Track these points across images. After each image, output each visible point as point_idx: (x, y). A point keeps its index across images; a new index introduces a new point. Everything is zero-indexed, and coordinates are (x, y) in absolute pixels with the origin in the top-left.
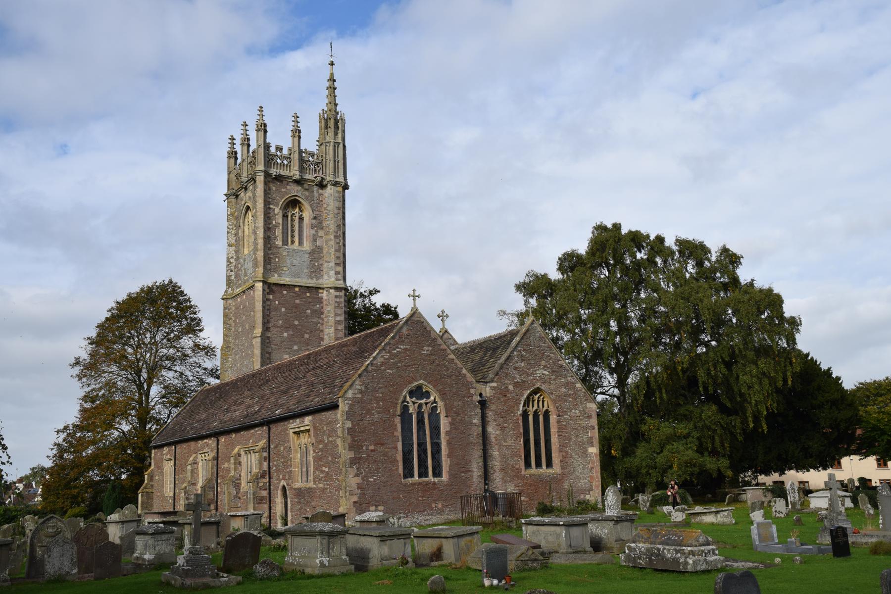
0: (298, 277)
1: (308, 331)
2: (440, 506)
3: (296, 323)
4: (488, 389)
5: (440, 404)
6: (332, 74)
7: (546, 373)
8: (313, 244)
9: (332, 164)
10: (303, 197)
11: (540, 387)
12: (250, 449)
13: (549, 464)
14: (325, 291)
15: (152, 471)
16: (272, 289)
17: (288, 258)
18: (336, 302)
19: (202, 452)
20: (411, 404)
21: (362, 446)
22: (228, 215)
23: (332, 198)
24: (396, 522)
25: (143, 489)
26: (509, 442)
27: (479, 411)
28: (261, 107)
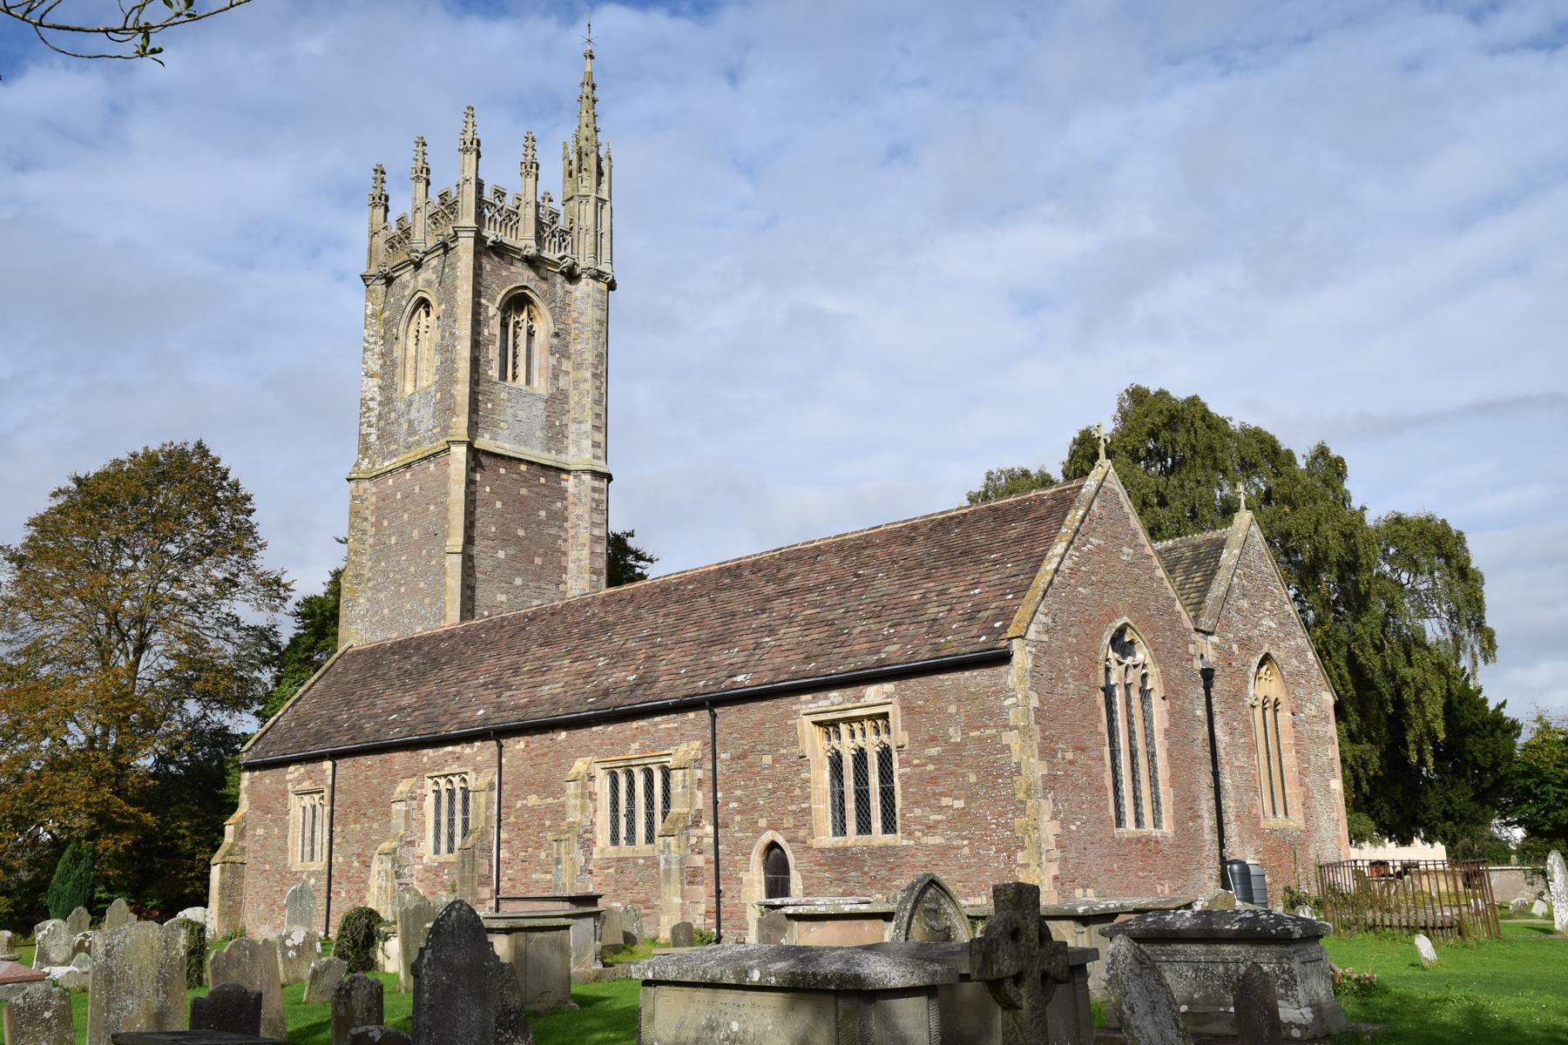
1: (541, 551)
3: (521, 533)
5: (1152, 670)
8: (552, 385)
9: (590, 238)
10: (537, 292)
12: (634, 763)
14: (571, 478)
15: (244, 817)
16: (480, 462)
17: (509, 404)
18: (593, 499)
19: (435, 773)
22: (366, 315)
23: (591, 300)
25: (224, 857)
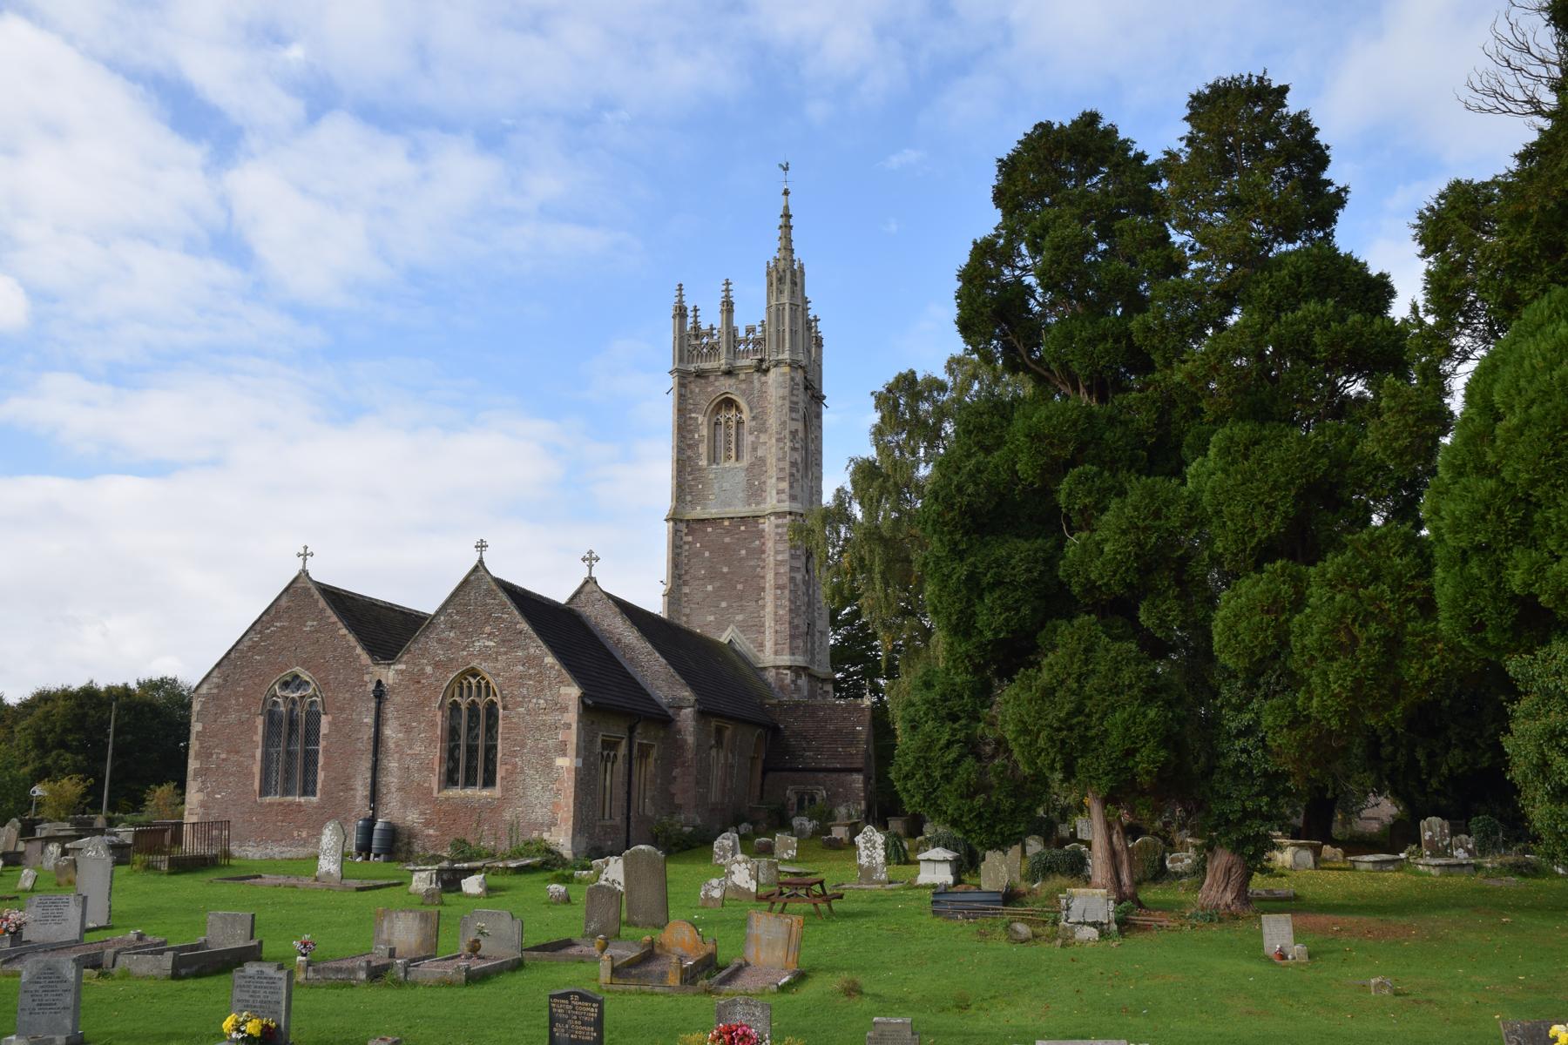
0: (730, 506)
2: (304, 834)
4: (391, 674)
6: (787, 208)
7: (492, 644)
18: (777, 534)
21: (212, 754)
26: (419, 748)
27: (373, 705)
28: (728, 284)
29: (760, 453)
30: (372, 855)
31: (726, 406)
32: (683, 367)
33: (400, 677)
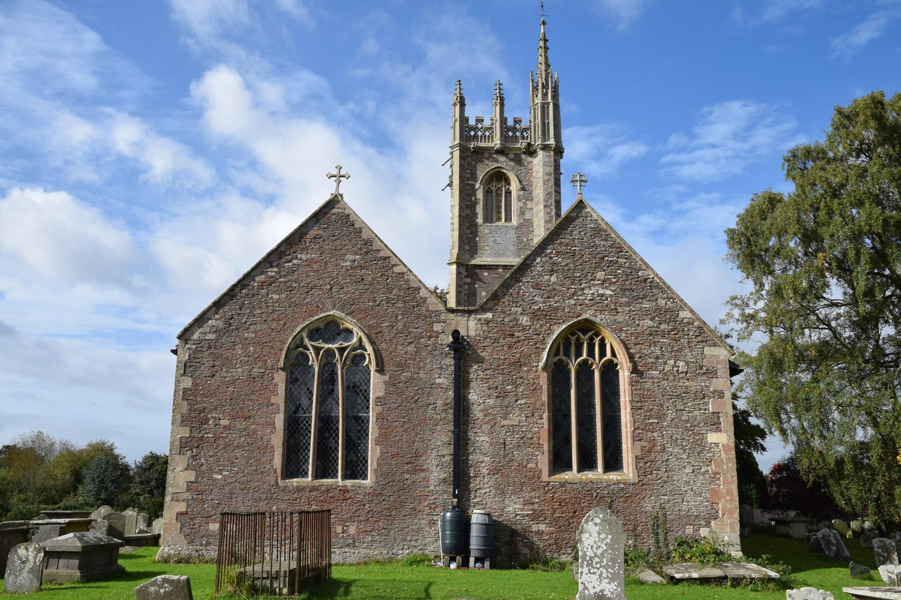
0: (502, 256)
2: (352, 530)
4: (472, 323)
7: (608, 292)
10: (508, 168)
11: (593, 319)
13: (613, 462)
17: (491, 236)
20: (311, 354)
21: (208, 420)
24: (31, 558)
27: (450, 361)
29: (527, 217)
30: (472, 560)
31: (496, 178)
32: (464, 143)
33: (485, 328)
